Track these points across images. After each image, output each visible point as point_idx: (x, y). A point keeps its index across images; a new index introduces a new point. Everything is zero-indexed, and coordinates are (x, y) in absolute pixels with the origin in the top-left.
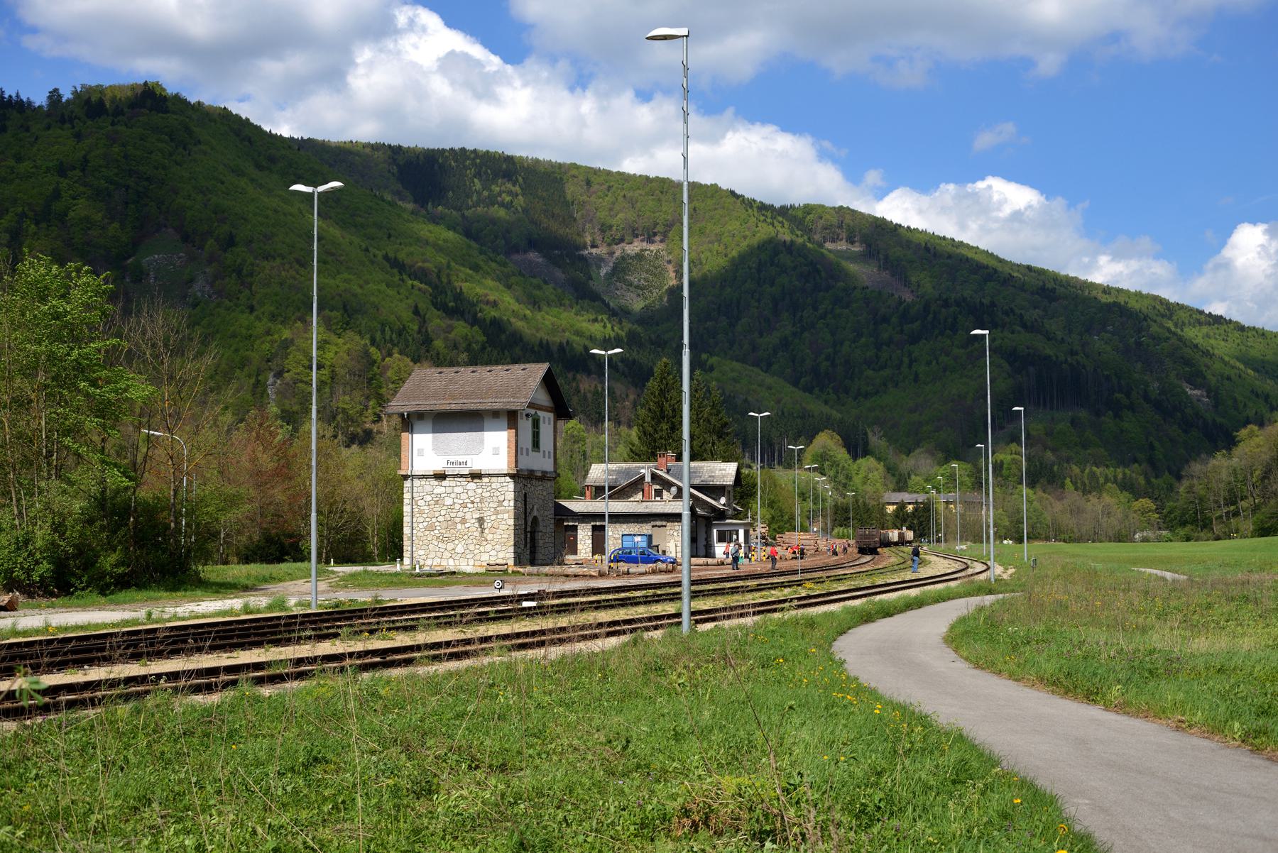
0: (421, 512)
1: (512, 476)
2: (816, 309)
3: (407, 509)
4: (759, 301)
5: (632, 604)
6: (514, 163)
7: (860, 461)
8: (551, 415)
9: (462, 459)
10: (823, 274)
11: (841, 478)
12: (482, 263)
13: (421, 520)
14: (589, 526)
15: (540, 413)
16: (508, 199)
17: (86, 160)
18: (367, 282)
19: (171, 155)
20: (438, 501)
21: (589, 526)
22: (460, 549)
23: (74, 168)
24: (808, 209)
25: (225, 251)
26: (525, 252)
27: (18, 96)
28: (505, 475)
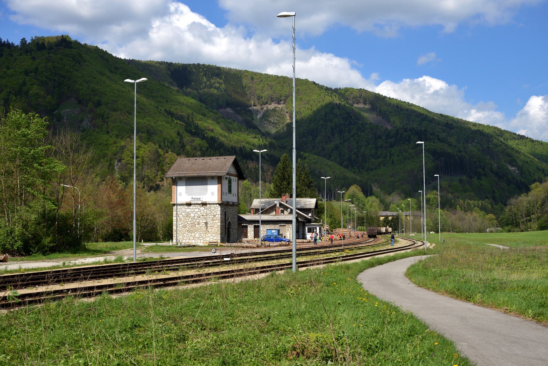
0: (181, 220)
1: (219, 204)
2: (350, 133)
3: (174, 218)
4: (325, 129)
5: (271, 259)
6: (220, 70)
7: (369, 198)
8: (236, 178)
9: (198, 197)
10: (353, 118)
11: (361, 205)
12: (206, 113)
13: (180, 223)
14: (253, 226)
15: (231, 177)
16: (218, 85)
17: (37, 69)
18: (157, 121)
19: (73, 66)
20: (188, 215)
21: (253, 226)
22: (197, 235)
23: (32, 72)
24: (347, 90)
25: (96, 108)
26: (225, 108)
27: (8, 41)
28: (217, 204)
